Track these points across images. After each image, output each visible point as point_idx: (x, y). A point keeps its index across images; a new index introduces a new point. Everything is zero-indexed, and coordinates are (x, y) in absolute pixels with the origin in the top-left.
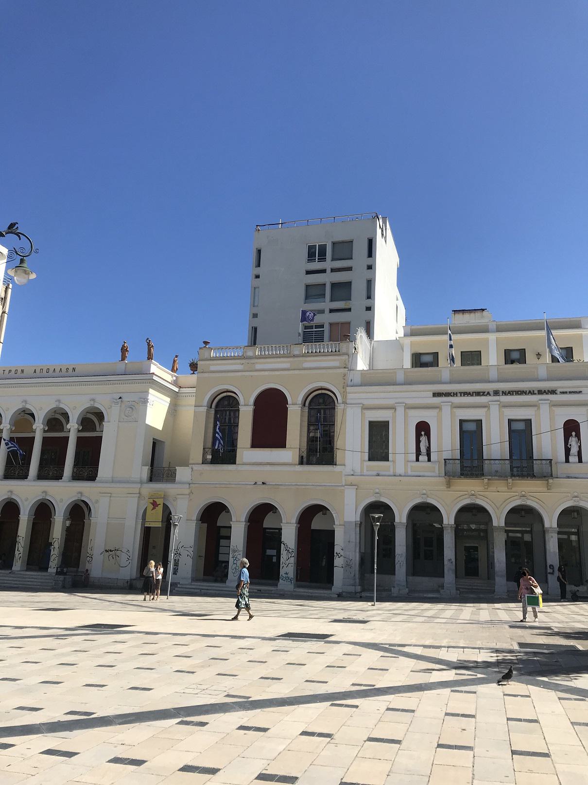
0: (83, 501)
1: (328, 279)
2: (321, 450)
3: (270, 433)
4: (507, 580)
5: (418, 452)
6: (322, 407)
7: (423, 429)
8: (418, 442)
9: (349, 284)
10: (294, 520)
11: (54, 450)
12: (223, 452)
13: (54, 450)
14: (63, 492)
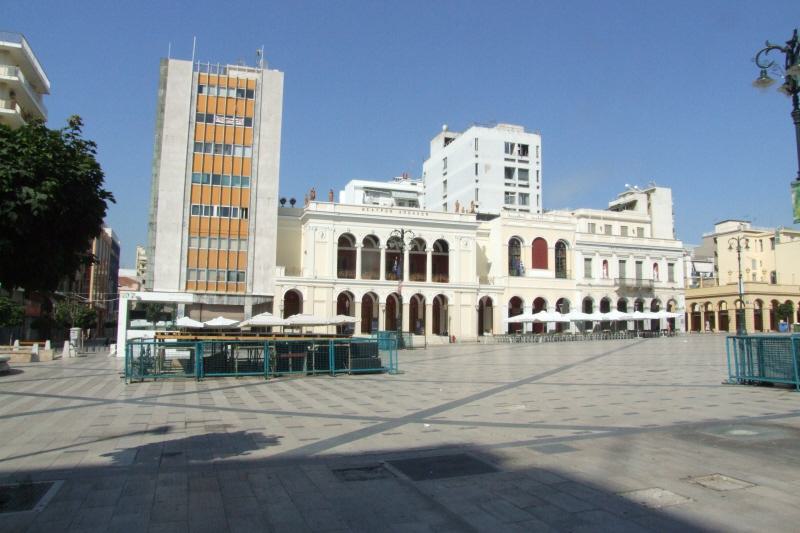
2: (561, 270)
11: (394, 257)
13: (394, 257)
14: (430, 290)
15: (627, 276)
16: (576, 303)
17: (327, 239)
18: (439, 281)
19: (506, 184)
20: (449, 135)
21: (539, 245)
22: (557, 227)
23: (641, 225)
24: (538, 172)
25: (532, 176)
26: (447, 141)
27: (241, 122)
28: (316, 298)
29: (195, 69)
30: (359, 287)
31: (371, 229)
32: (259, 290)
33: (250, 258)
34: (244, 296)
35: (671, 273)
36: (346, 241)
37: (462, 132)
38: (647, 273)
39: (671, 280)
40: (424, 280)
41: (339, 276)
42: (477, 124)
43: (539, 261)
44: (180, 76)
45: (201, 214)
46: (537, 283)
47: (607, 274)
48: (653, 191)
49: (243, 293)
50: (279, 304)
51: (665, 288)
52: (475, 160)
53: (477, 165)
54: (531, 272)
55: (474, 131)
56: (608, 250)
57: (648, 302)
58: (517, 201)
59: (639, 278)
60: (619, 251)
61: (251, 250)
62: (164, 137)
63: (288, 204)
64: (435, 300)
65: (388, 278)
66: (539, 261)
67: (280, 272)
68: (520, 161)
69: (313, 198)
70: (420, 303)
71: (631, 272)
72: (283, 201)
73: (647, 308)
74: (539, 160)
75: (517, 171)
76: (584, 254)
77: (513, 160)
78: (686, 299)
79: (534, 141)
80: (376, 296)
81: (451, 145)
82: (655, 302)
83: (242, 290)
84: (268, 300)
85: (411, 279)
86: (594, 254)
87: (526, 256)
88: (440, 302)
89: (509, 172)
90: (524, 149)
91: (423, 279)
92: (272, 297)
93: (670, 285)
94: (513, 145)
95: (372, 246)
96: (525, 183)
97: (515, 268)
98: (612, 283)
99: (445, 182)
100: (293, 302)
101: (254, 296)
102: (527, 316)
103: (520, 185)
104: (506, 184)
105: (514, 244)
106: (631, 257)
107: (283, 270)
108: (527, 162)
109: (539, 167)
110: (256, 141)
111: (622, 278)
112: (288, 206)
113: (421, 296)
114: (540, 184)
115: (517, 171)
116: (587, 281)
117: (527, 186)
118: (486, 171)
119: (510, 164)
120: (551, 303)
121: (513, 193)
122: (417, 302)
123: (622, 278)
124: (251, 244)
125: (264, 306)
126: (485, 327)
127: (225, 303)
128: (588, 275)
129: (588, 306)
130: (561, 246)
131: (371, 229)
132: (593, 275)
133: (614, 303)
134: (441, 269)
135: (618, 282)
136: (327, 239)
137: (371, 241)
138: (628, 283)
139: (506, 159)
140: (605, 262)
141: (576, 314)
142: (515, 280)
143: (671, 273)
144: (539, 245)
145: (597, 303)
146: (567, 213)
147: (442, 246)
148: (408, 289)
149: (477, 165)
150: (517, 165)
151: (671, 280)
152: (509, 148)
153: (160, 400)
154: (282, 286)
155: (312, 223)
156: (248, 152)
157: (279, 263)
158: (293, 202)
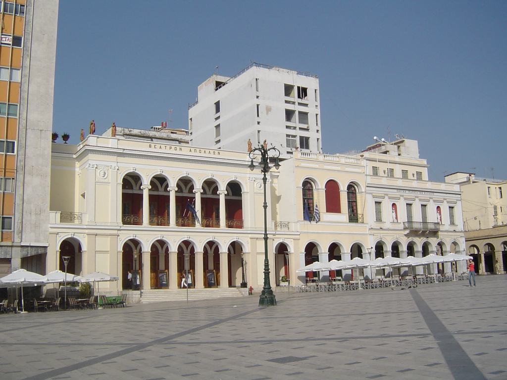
2: (354, 217)
13: (185, 204)
14: (224, 237)
15: (429, 220)
17: (110, 179)
18: (183, 225)
19: (287, 127)
20: (221, 79)
21: (332, 187)
22: (347, 169)
23: (419, 169)
24: (317, 115)
25: (311, 119)
26: (219, 85)
27: (8, 40)
28: (96, 250)
30: (147, 234)
32: (30, 239)
33: (18, 201)
34: (12, 246)
35: (452, 216)
36: (131, 181)
37: (235, 77)
38: (432, 217)
39: (452, 223)
40: (139, 223)
41: (124, 223)
42: (258, 65)
43: (333, 206)
46: (332, 228)
47: (397, 218)
48: (403, 141)
49: (10, 244)
50: (53, 258)
51: (388, 230)
52: (257, 101)
53: (258, 106)
55: (254, 72)
56: (411, 195)
57: (434, 246)
59: (425, 222)
60: (407, 194)
61: (19, 191)
63: (60, 140)
64: (154, 247)
66: (333, 206)
67: (55, 216)
68: (300, 104)
69: (93, 132)
70: (162, 253)
71: (417, 217)
72: (55, 136)
73: (418, 252)
74: (318, 103)
75: (297, 113)
77: (294, 103)
78: (466, 241)
79: (311, 84)
81: (223, 88)
82: (440, 244)
83: (7, 239)
84: (40, 251)
85: (151, 223)
87: (320, 199)
88: (235, 248)
89: (289, 114)
90: (303, 92)
91: (139, 223)
92: (46, 247)
93: (452, 228)
96: (305, 126)
97: (309, 213)
98: (401, 226)
99: (218, 127)
100: (71, 254)
101: (22, 246)
102: (324, 265)
103: (300, 129)
104: (287, 127)
105: (307, 186)
106: (417, 200)
107: (58, 215)
108: (306, 105)
109: (318, 111)
110: (27, 63)
111: (410, 221)
112: (61, 139)
113: (162, 243)
114: (319, 128)
115: (297, 113)
116: (380, 223)
117: (307, 130)
118: (267, 113)
119: (290, 107)
120: (323, 251)
121: (295, 136)
122: (160, 248)
123: (410, 221)
124: (20, 184)
125: (35, 261)
127: (189, 259)
128: (379, 219)
129: (379, 251)
130: (351, 188)
132: (384, 219)
133: (403, 248)
135: (407, 225)
136: (110, 179)
138: (416, 226)
140: (394, 205)
142: (312, 226)
143: (452, 216)
144: (332, 187)
145: (388, 248)
146: (358, 156)
147: (235, 188)
149: (258, 106)
150: (298, 108)
151: (452, 223)
152: (288, 89)
154: (57, 234)
155: (92, 159)
156: (17, 76)
157: (53, 208)
158: (66, 137)
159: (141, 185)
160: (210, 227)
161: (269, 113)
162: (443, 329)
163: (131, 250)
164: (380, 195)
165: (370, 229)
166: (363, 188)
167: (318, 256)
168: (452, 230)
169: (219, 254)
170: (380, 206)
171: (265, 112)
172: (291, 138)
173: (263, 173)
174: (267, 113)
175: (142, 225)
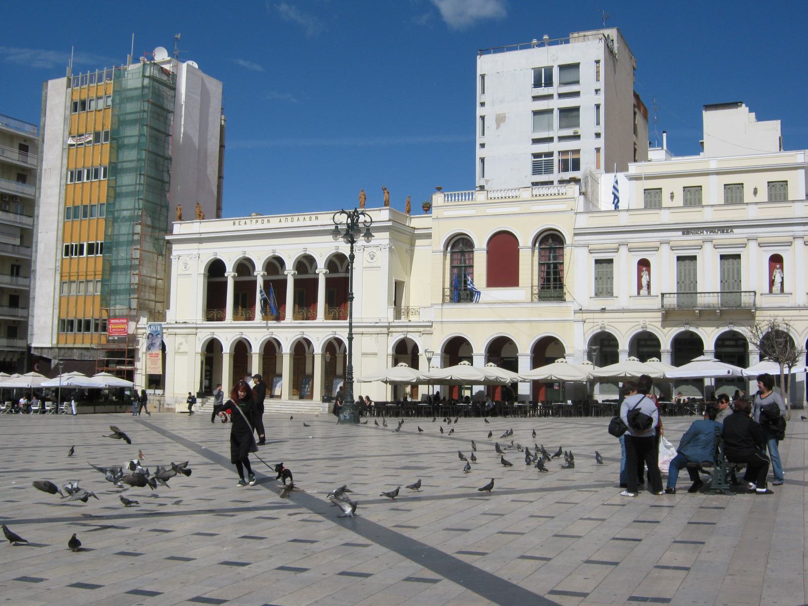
0: (274, 339)
1: (557, 104)
2: (552, 284)
3: (503, 270)
4: (19, 149)
5: (640, 287)
6: (551, 242)
7: (644, 264)
8: (640, 278)
9: (576, 109)
10: (529, 352)
11: (276, 287)
12: (461, 291)
13: (276, 287)
14: (319, 331)
16: (576, 342)
18: (334, 318)
25: (587, 118)
29: (69, 86)
30: (227, 333)
31: (212, 251)
36: (216, 268)
44: (57, 94)
45: (97, 253)
46: (509, 311)
51: (623, 311)
54: (490, 295)
58: (556, 168)
60: (765, 234)
62: (43, 171)
65: (295, 318)
71: (709, 279)
76: (591, 252)
80: (309, 343)
86: (744, 246)
87: (529, 265)
91: (251, 318)
94: (549, 71)
95: (306, 272)
98: (656, 303)
117: (577, 137)
118: (498, 127)
120: (479, 348)
121: (551, 154)
122: (302, 348)
126: (605, 385)
131: (212, 251)
134: (340, 296)
137: (245, 266)
139: (535, 98)
141: (526, 375)
148: (287, 332)
153: (793, 436)
159: (316, 268)
160: (213, 320)
161: (502, 125)
162: (235, 439)
163: (212, 348)
164: (693, 243)
165: (575, 312)
166: (568, 239)
167: (517, 358)
168: (599, 308)
169: (418, 356)
170: (612, 268)
171: (494, 125)
172: (543, 159)
173: (350, 245)
174: (498, 127)
175: (253, 320)
